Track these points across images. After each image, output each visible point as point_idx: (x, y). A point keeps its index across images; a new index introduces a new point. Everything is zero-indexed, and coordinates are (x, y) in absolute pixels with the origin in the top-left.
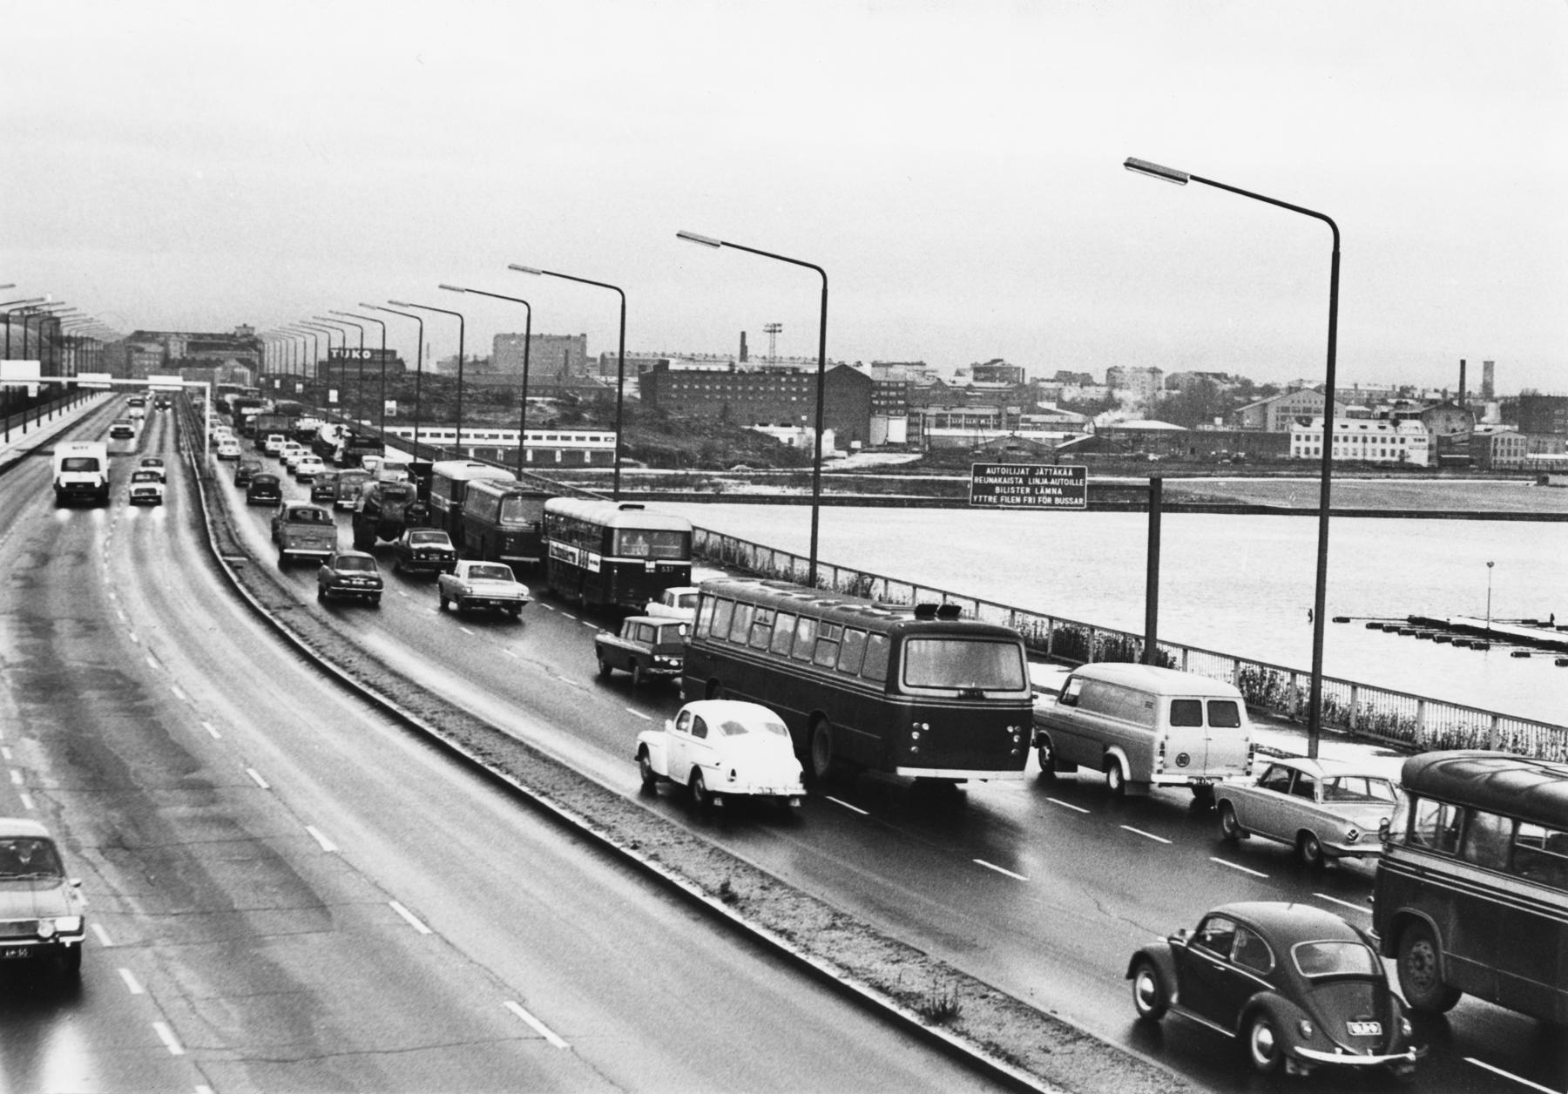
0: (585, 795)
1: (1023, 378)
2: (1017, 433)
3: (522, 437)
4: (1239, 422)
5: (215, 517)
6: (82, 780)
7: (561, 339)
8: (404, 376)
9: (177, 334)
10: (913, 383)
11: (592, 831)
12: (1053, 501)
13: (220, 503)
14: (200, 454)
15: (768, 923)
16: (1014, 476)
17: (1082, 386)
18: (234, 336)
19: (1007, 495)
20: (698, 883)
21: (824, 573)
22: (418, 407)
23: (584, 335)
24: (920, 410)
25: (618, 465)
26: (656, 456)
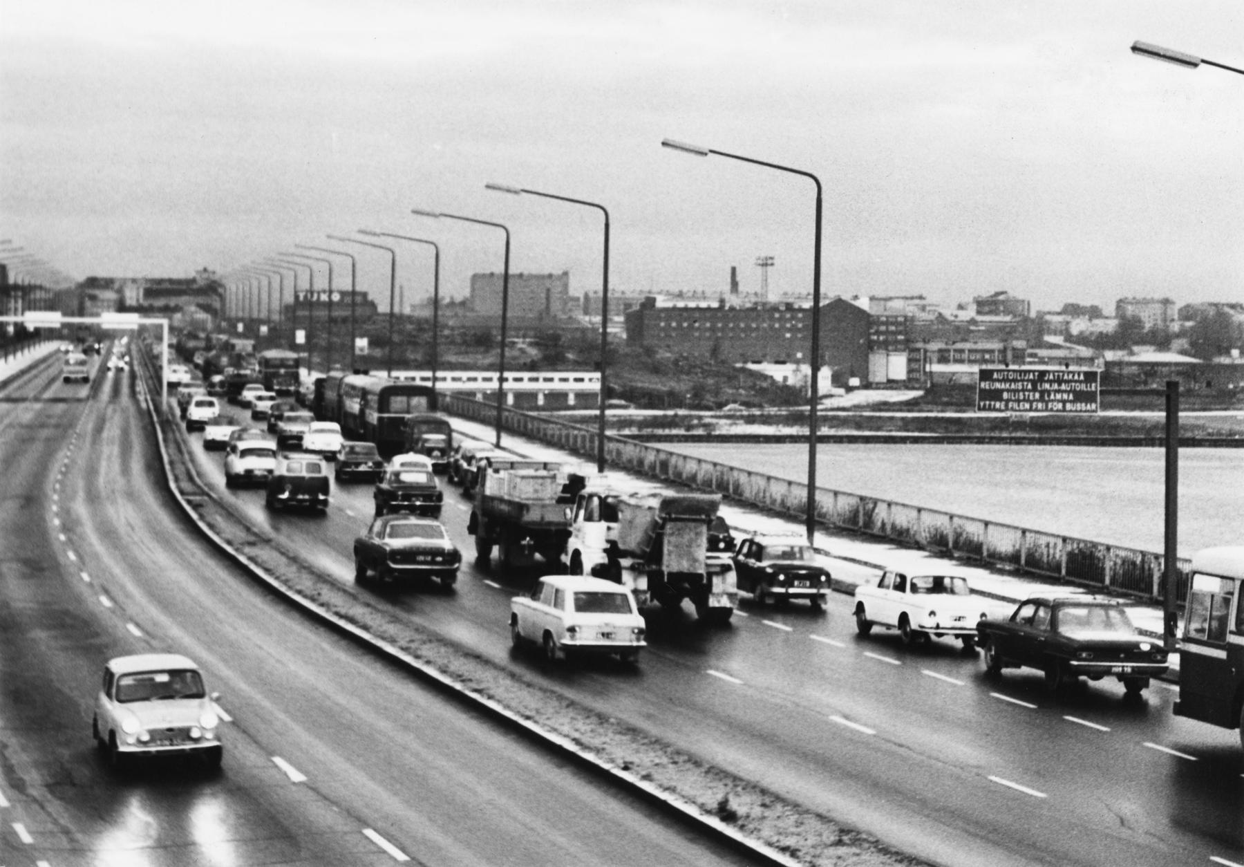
0: (573, 719)
1: (1029, 310)
3: (502, 380)
9: (134, 281)
10: (913, 319)
12: (1064, 406)
14: (157, 398)
15: (770, 840)
17: (1090, 320)
19: (1015, 401)
20: (694, 802)
21: (825, 502)
23: (566, 274)
24: (920, 345)
25: (603, 408)
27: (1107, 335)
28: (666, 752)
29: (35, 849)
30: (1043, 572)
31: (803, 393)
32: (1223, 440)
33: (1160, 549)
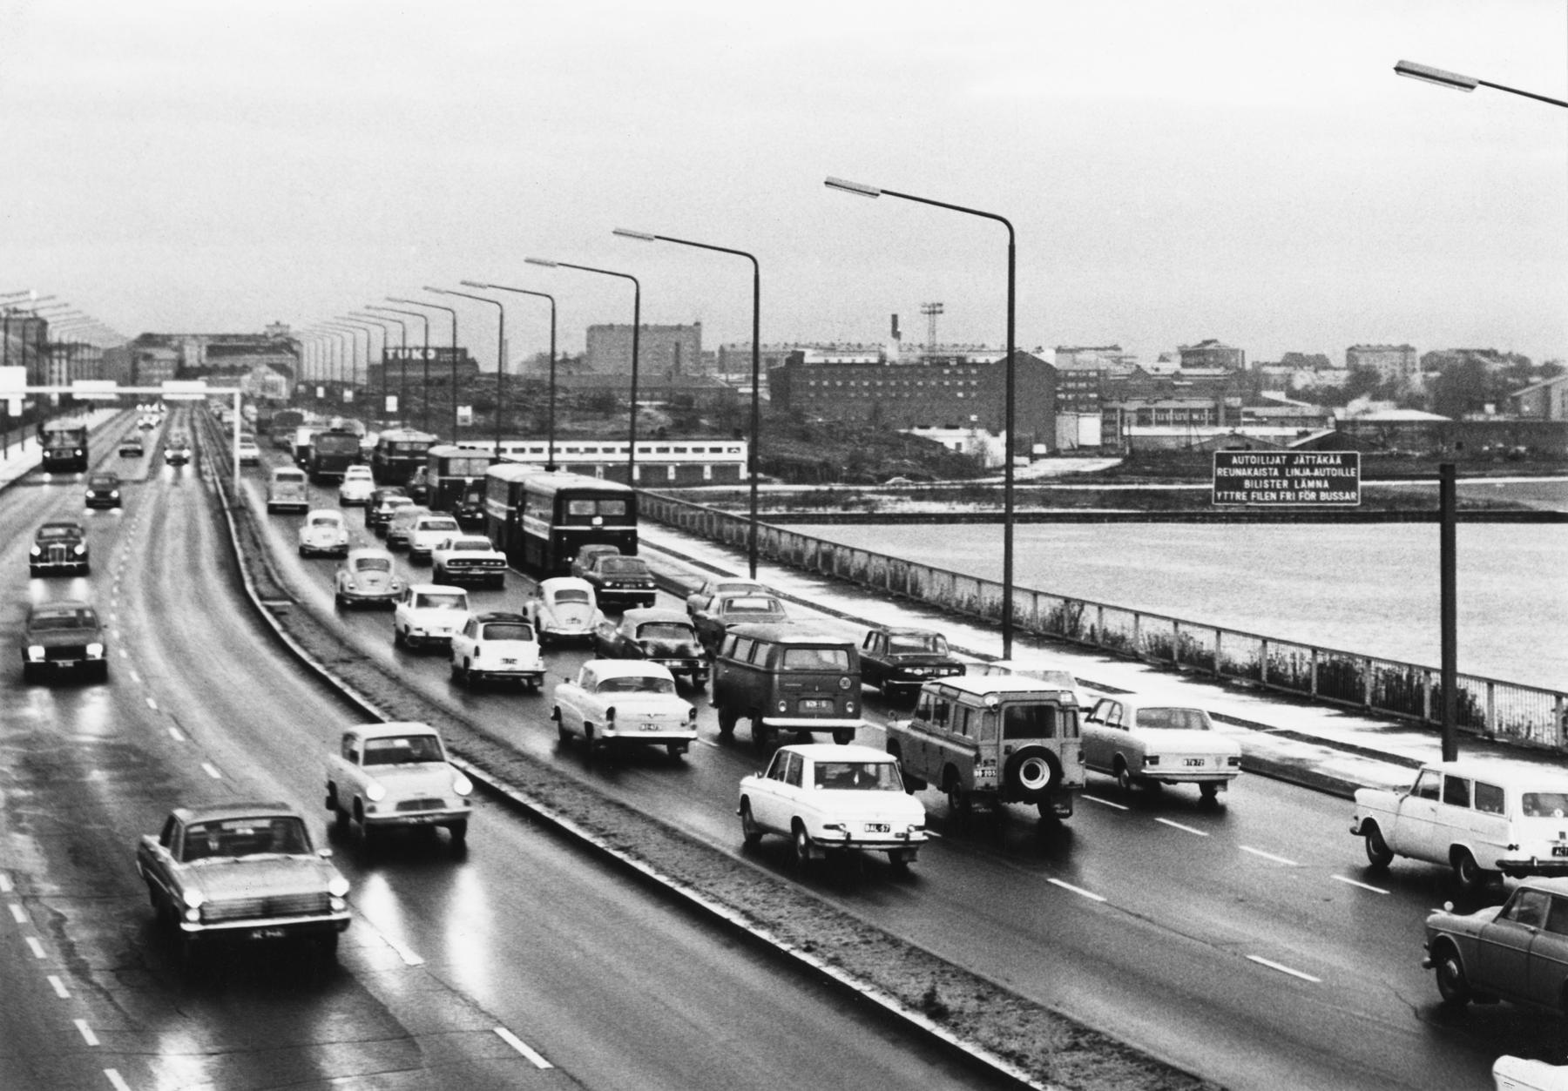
1: (1243, 363)
2: (1239, 430)
4: (1517, 409)
5: (250, 554)
6: (89, 883)
7: (672, 329)
8: (477, 379)
9: (195, 336)
11: (752, 930)
13: (257, 542)
14: (227, 479)
16: (1267, 466)
18: (265, 336)
20: (895, 994)
21: (1023, 604)
22: (498, 415)
24: (1115, 404)
26: (792, 470)
27: (1335, 389)
28: (856, 929)
29: (101, 1053)
30: (1286, 689)
31: (980, 463)
32: (1479, 513)
33: (1436, 662)
